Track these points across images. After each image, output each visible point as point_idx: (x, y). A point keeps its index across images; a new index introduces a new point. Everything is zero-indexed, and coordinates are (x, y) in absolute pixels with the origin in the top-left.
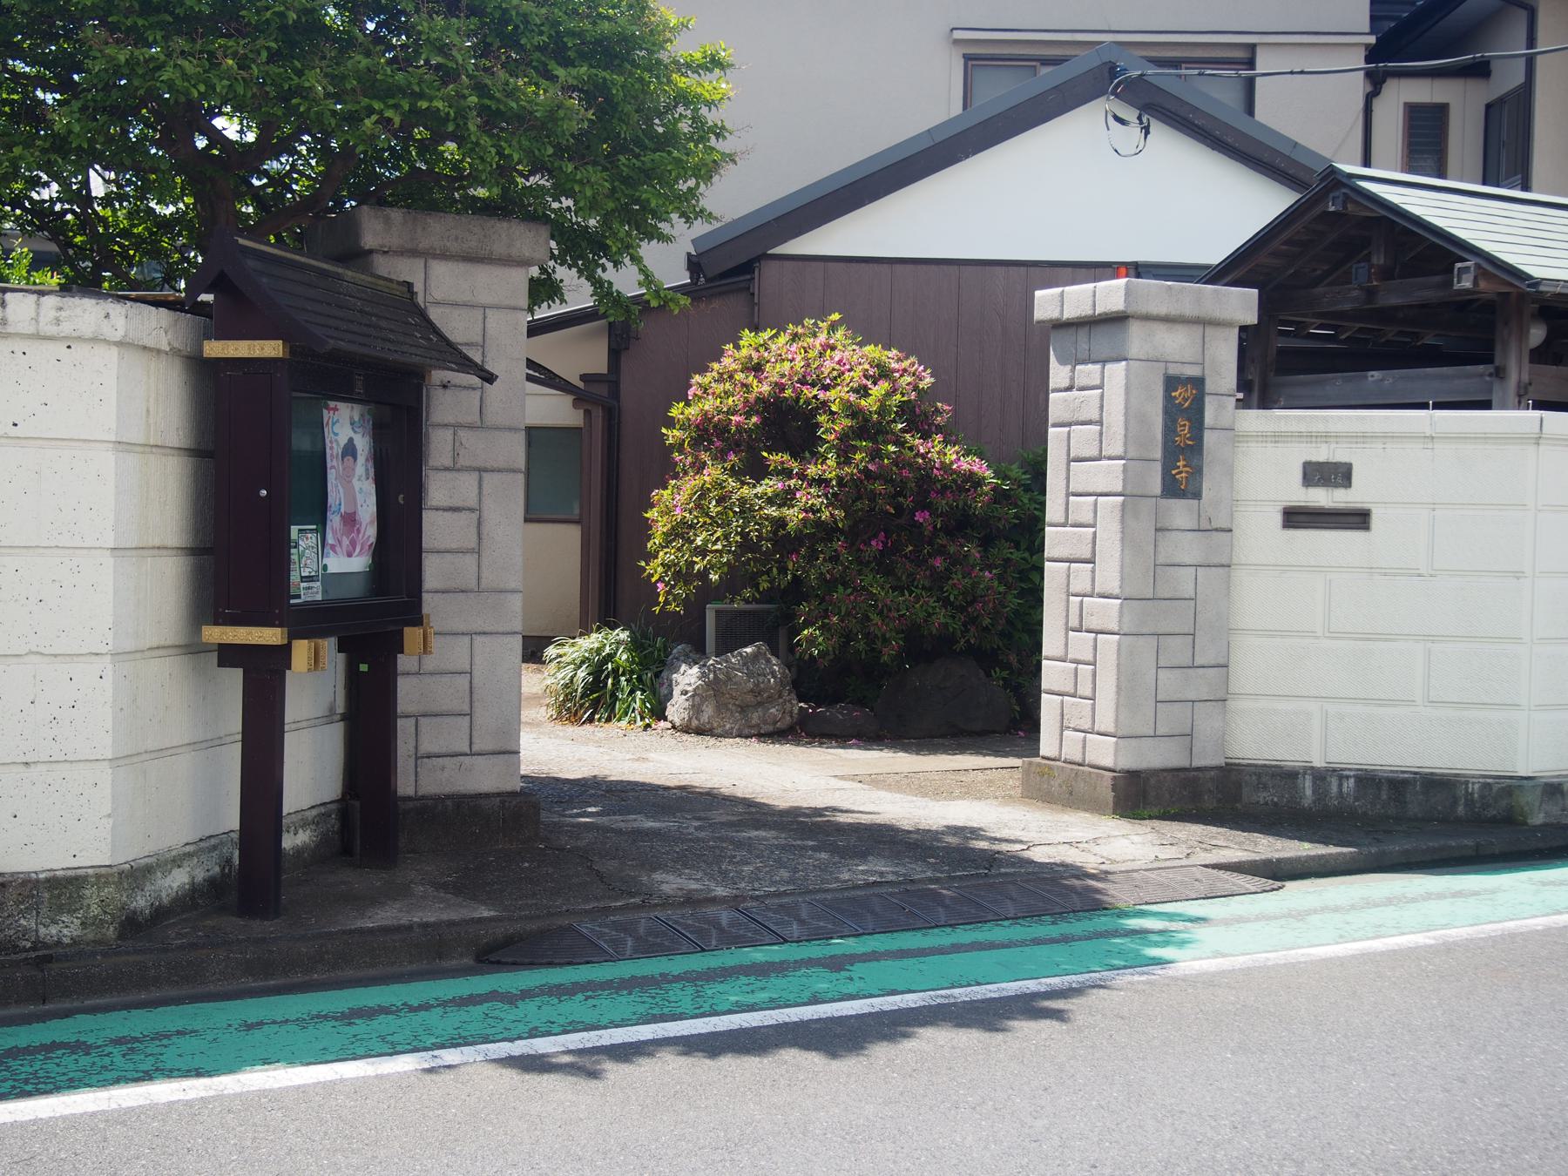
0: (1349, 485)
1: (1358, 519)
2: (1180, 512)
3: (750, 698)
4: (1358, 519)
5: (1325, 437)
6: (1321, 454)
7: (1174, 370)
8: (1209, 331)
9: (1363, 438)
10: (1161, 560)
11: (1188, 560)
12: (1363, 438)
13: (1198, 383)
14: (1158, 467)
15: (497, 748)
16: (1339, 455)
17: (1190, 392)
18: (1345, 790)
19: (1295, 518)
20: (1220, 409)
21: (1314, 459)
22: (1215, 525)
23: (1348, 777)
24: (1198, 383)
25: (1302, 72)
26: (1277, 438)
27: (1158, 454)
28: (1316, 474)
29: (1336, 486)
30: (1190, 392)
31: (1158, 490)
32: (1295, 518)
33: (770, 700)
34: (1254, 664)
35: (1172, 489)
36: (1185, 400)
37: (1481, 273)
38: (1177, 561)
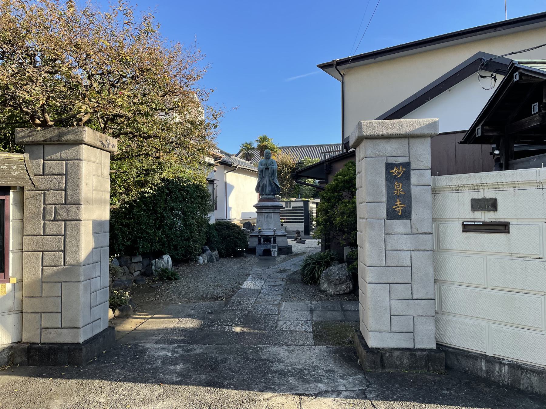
0: (496, 210)
1: (502, 227)
2: (399, 225)
3: (338, 282)
4: (502, 227)
5: (482, 186)
6: (479, 195)
7: (391, 160)
8: (412, 140)
9: (502, 186)
10: (389, 248)
11: (404, 248)
12: (502, 186)
13: (407, 165)
14: (385, 205)
15: (71, 326)
16: (489, 195)
17: (402, 170)
18: (503, 371)
19: (467, 228)
20: (421, 177)
21: (476, 197)
22: (420, 231)
23: (505, 364)
24: (407, 165)
25: (525, 50)
26: (459, 188)
27: (384, 199)
28: (478, 205)
29: (489, 211)
30: (402, 170)
31: (385, 215)
32: (467, 228)
33: (343, 282)
34: (457, 297)
35: (392, 215)
36: (399, 173)
37: (521, 74)
38: (399, 248)
